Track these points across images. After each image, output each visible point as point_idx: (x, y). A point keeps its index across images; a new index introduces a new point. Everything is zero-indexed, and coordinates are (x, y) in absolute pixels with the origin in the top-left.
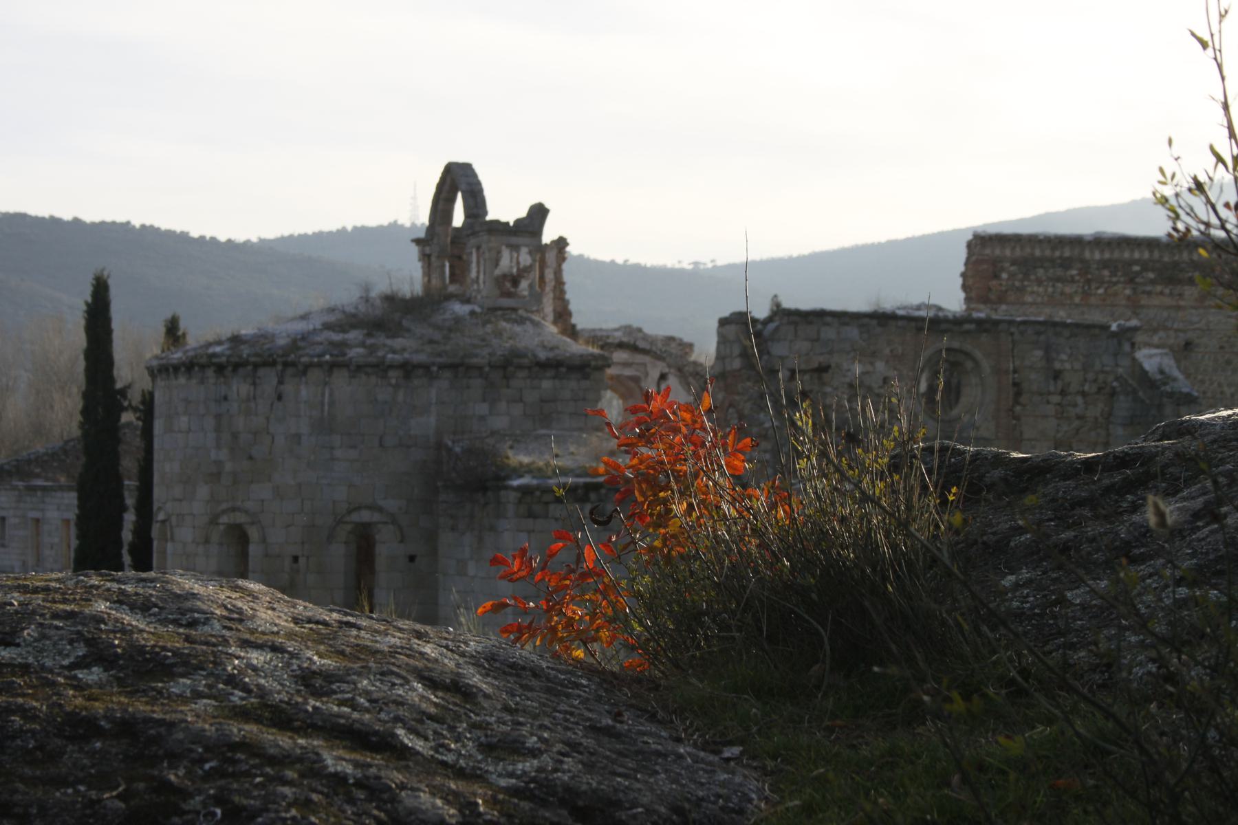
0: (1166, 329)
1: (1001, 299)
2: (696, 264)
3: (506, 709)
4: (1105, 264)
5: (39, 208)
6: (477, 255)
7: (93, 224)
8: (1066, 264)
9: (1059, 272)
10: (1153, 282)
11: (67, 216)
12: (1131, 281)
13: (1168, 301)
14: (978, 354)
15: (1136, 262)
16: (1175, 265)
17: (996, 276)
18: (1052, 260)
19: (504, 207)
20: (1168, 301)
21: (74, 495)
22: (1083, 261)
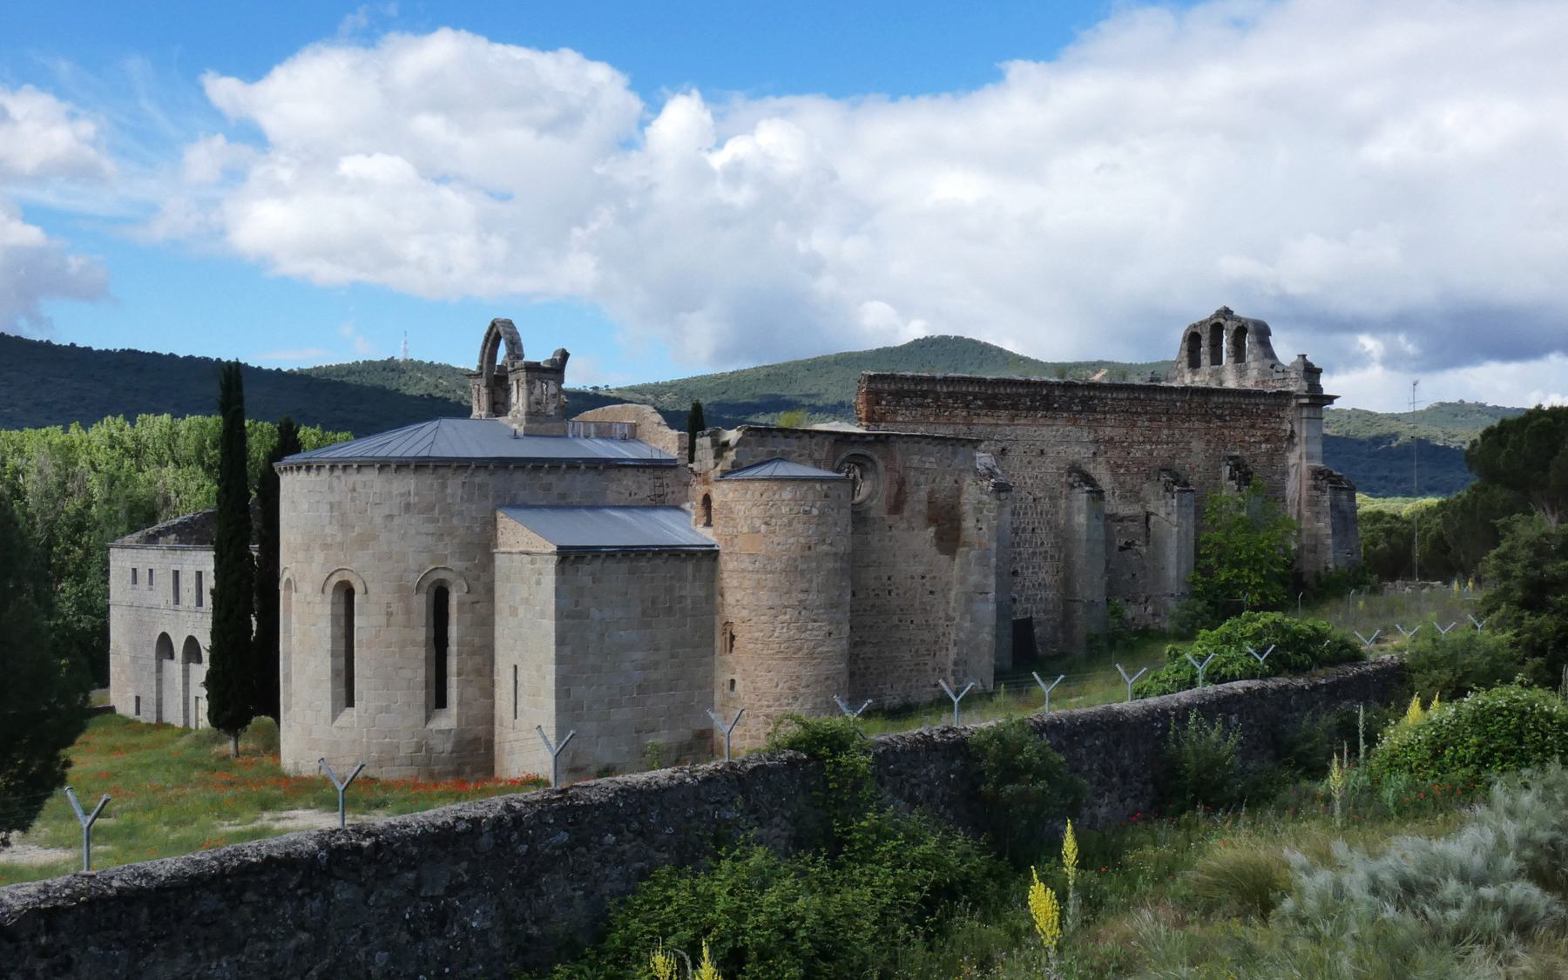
0: (989, 439)
1: (882, 419)
2: (596, 388)
3: (1028, 969)
4: (949, 395)
5: (146, 347)
6: (73, 345)
7: (100, 352)
8: (925, 395)
9: (919, 401)
10: (981, 407)
11: (165, 352)
12: (967, 406)
13: (992, 421)
14: (876, 457)
15: (970, 394)
16: (995, 396)
17: (878, 403)
18: (915, 393)
19: (537, 351)
20: (992, 421)
21: (203, 562)
22: (935, 393)
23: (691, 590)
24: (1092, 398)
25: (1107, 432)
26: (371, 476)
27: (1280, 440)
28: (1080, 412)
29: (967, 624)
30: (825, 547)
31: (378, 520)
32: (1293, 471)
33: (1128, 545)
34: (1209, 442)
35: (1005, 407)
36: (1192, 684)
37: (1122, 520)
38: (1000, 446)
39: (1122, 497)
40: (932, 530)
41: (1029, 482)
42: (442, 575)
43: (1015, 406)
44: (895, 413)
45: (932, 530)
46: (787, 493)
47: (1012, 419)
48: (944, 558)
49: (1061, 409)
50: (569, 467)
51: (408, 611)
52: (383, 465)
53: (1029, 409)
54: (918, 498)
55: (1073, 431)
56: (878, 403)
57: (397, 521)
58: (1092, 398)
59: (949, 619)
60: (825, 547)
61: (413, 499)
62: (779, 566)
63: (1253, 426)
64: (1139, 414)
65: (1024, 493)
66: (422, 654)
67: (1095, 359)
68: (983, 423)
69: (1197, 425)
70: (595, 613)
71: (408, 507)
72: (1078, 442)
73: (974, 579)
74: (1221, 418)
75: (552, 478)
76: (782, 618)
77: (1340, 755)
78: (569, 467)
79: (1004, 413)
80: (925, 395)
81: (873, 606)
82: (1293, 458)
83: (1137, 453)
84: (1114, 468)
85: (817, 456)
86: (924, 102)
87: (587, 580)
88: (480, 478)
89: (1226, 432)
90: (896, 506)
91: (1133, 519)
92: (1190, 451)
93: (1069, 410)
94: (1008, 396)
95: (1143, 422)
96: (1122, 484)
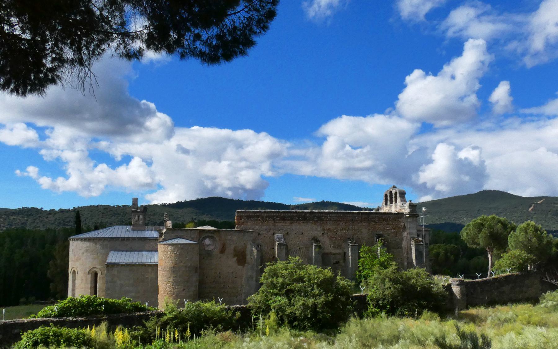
1: (243, 224)
4: (267, 217)
8: (258, 217)
9: (256, 218)
10: (279, 220)
17: (241, 220)
23: (150, 276)
24: (322, 216)
25: (328, 227)
26: (79, 242)
27: (400, 228)
28: (317, 221)
29: (248, 287)
30: (182, 264)
31: (81, 254)
32: (405, 238)
33: (337, 263)
34: (369, 229)
35: (288, 220)
36: (50, 317)
37: (334, 254)
38: (286, 232)
39: (334, 247)
40: (236, 258)
41: (298, 243)
42: (95, 269)
43: (292, 219)
44: (247, 222)
45: (236, 258)
46: (170, 248)
47: (291, 223)
48: (240, 267)
49: (309, 220)
50: (127, 240)
51: (86, 280)
52: (82, 240)
53: (297, 220)
54: (230, 249)
55: (315, 227)
56: (241, 220)
57: (85, 254)
58: (322, 216)
59: (242, 286)
60: (182, 264)
61: (88, 248)
62: (168, 269)
63: (388, 224)
64: (341, 221)
65: (295, 246)
66: (89, 291)
67: (541, 196)
68: (280, 224)
69: (364, 224)
70: (119, 282)
71: (87, 251)
72: (316, 230)
73: (249, 274)
74: (374, 221)
75: (127, 243)
76: (168, 285)
77: (259, 334)
78: (127, 240)
79: (287, 222)
80: (258, 217)
81: (214, 281)
82: (405, 234)
83: (340, 233)
84: (331, 238)
85: (193, 236)
86: (332, 121)
87: (116, 272)
88: (106, 243)
89: (377, 226)
90: (222, 251)
91: (339, 254)
92: (361, 232)
93: (313, 220)
94: (289, 216)
95: (342, 223)
96: (334, 243)
